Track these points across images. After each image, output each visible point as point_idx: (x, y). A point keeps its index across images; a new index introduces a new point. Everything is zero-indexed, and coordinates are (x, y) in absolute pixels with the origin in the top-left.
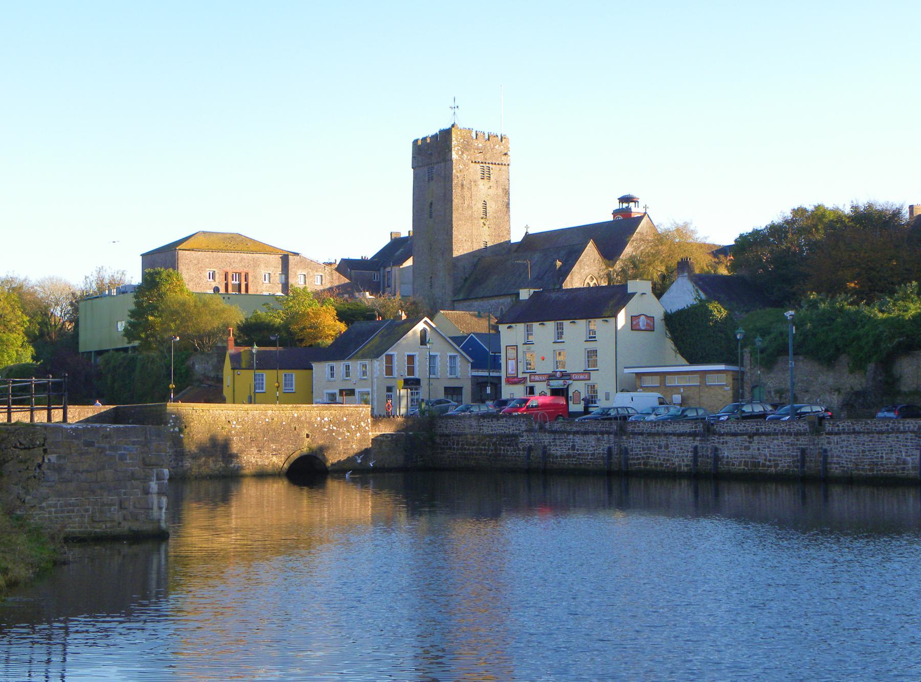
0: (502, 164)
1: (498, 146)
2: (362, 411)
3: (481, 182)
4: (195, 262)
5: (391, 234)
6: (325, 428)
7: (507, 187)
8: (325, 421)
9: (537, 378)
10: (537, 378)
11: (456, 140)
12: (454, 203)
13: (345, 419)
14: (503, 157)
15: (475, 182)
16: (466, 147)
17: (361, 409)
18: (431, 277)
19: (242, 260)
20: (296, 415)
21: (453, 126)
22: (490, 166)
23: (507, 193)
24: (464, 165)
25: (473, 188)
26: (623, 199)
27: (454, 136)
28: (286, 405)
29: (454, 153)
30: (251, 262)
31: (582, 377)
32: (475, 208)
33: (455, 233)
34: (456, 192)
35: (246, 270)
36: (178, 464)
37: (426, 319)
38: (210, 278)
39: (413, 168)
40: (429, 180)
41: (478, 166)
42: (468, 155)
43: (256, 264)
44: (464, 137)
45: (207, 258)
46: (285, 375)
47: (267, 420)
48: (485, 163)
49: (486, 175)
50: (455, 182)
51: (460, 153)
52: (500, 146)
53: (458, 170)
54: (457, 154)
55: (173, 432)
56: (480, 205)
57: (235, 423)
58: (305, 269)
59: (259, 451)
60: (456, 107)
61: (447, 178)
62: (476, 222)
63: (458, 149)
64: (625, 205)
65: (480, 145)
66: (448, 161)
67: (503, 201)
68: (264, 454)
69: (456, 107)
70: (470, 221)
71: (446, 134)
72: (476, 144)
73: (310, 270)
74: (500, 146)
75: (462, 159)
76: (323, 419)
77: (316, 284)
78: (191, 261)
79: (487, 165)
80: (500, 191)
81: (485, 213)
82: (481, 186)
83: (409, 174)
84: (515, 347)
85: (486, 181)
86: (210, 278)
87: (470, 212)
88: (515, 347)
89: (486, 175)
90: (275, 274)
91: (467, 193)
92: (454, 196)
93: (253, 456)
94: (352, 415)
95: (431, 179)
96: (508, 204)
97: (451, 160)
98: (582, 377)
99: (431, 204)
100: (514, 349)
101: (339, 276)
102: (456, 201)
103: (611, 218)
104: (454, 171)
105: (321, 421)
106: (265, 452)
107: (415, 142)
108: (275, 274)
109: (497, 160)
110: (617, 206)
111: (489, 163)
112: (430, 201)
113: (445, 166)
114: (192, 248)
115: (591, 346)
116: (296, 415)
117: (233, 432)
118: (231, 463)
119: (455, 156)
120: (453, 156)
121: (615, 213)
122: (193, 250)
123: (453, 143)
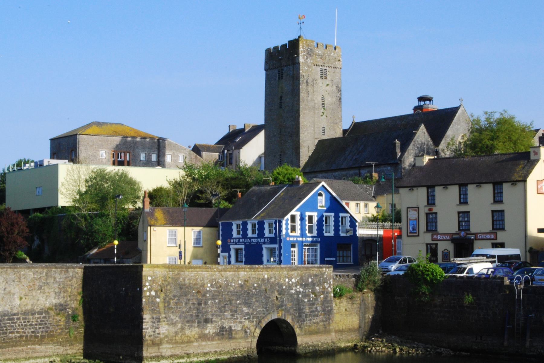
1: (333, 53)
2: (326, 271)
3: (320, 81)
4: (91, 144)
5: (229, 127)
6: (292, 289)
7: (340, 86)
8: (293, 282)
9: (439, 237)
10: (439, 237)
11: (303, 47)
12: (301, 97)
13: (310, 280)
14: (337, 63)
15: (316, 81)
16: (310, 53)
17: (324, 269)
18: (281, 155)
20: (266, 276)
21: (299, 37)
22: (327, 68)
23: (339, 90)
24: (309, 67)
25: (315, 85)
26: (421, 99)
27: (300, 42)
28: (257, 266)
29: (301, 57)
30: (132, 145)
31: (487, 236)
32: (316, 101)
33: (301, 120)
34: (303, 87)
36: (154, 332)
37: (323, 183)
39: (265, 70)
40: (279, 79)
41: (319, 69)
42: (311, 60)
44: (308, 46)
45: (100, 141)
46: (170, 231)
47: (240, 282)
49: (324, 75)
51: (305, 58)
52: (334, 54)
55: (149, 296)
56: (319, 99)
57: (209, 285)
58: (171, 150)
59: (232, 315)
60: (302, 22)
61: (295, 78)
62: (317, 112)
63: (304, 55)
64: (422, 103)
66: (296, 64)
67: (337, 96)
68: (237, 318)
69: (302, 22)
70: (312, 111)
71: (294, 45)
73: (175, 151)
74: (334, 54)
75: (307, 62)
76: (291, 280)
77: (179, 162)
78: (88, 143)
79: (325, 68)
80: (334, 88)
81: (323, 105)
82: (321, 85)
83: (262, 75)
84: (417, 209)
87: (313, 103)
88: (417, 209)
89: (324, 75)
91: (310, 89)
92: (301, 91)
93: (227, 320)
94: (316, 275)
95: (281, 77)
96: (340, 99)
97: (299, 63)
98: (487, 236)
99: (281, 97)
100: (416, 210)
101: (196, 156)
102: (302, 95)
103: (412, 112)
104: (301, 71)
105: (288, 282)
106: (238, 316)
107: (268, 51)
110: (416, 103)
112: (280, 95)
114: (89, 134)
115: (463, 208)
116: (266, 276)
117: (208, 295)
118: (207, 329)
119: (301, 60)
121: (415, 109)
122: (90, 135)
123: (300, 50)
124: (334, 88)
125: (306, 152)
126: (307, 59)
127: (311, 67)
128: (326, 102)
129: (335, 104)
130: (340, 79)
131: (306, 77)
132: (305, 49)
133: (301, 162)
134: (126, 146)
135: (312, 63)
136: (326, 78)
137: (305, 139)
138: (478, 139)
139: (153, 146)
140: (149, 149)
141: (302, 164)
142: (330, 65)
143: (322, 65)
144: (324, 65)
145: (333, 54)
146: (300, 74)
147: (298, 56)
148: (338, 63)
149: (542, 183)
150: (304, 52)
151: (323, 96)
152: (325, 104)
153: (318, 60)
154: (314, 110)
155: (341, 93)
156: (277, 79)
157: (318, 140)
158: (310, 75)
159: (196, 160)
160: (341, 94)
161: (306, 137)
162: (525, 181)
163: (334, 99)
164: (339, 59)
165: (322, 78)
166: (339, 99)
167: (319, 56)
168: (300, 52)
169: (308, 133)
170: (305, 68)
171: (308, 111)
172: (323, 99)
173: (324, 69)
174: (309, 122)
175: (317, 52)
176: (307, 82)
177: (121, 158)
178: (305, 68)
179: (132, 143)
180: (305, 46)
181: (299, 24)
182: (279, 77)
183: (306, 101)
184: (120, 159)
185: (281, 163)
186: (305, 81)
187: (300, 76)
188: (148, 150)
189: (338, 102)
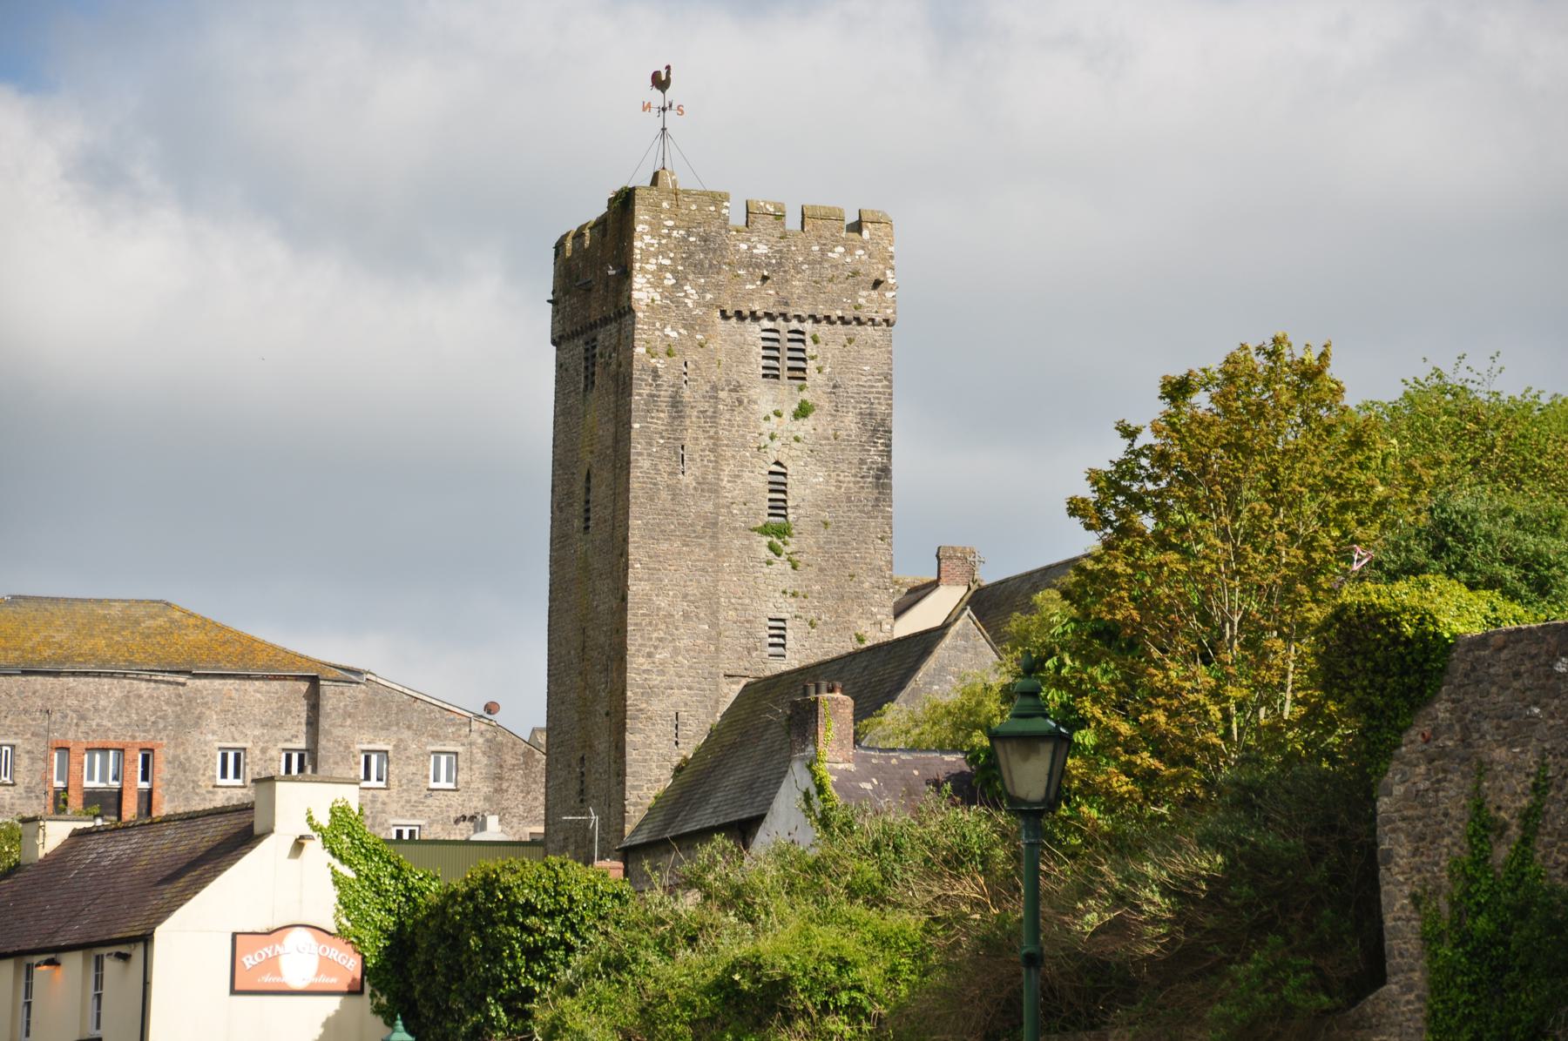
0: (859, 322)
11: (655, 230)
12: (635, 473)
14: (863, 296)
19: (126, 702)
22: (808, 326)
23: (879, 430)
29: (638, 281)
35: (142, 738)
38: (224, 775)
39: (554, 342)
41: (754, 331)
42: (702, 290)
43: (188, 719)
48: (784, 316)
50: (641, 392)
51: (670, 281)
52: (849, 251)
53: (661, 347)
54: (657, 283)
56: (759, 481)
58: (386, 728)
63: (661, 268)
65: (762, 249)
67: (862, 462)
70: (706, 542)
72: (744, 247)
73: (407, 734)
74: (849, 251)
75: (679, 303)
77: (433, 785)
79: (795, 324)
81: (779, 507)
85: (785, 386)
86: (224, 775)
87: (709, 507)
90: (264, 751)
91: (693, 435)
104: (640, 350)
108: (264, 751)
109: (834, 303)
111: (799, 318)
113: (619, 331)
119: (642, 291)
120: (636, 295)
123: (637, 244)
124: (850, 422)
125: (664, 746)
126: (678, 286)
127: (704, 326)
128: (795, 494)
129: (849, 500)
130: (887, 377)
131: (667, 378)
132: (669, 236)
133: (631, 796)
134: (135, 717)
135: (709, 305)
136: (798, 374)
137: (656, 679)
138: (1174, 682)
139: (289, 712)
140: (264, 725)
141: (635, 804)
142: (821, 311)
143: (774, 311)
144: (782, 309)
145: (844, 255)
146: (636, 365)
147: (626, 274)
148: (874, 294)
149: (280, 942)
150: (661, 252)
151: (777, 463)
152: (790, 503)
153: (749, 287)
154: (714, 537)
155: (888, 445)
156: (582, 386)
157: (744, 682)
158: (695, 362)
159: (526, 776)
160: (887, 452)
161: (662, 673)
162: (146, 939)
163: (848, 479)
164: (876, 275)
165: (777, 377)
166: (878, 478)
167: (758, 266)
168: (637, 254)
169: (676, 652)
170: (668, 330)
171: (677, 544)
172: (778, 484)
173: (783, 331)
174: (685, 596)
175: (744, 247)
176: (676, 403)
177: (103, 778)
178: (668, 330)
179: (167, 703)
180: (670, 223)
181: (667, 105)
182: (586, 386)
183: (665, 495)
184: (101, 781)
185: (582, 801)
186: (665, 394)
187: (636, 374)
188: (257, 732)
189: (869, 493)
